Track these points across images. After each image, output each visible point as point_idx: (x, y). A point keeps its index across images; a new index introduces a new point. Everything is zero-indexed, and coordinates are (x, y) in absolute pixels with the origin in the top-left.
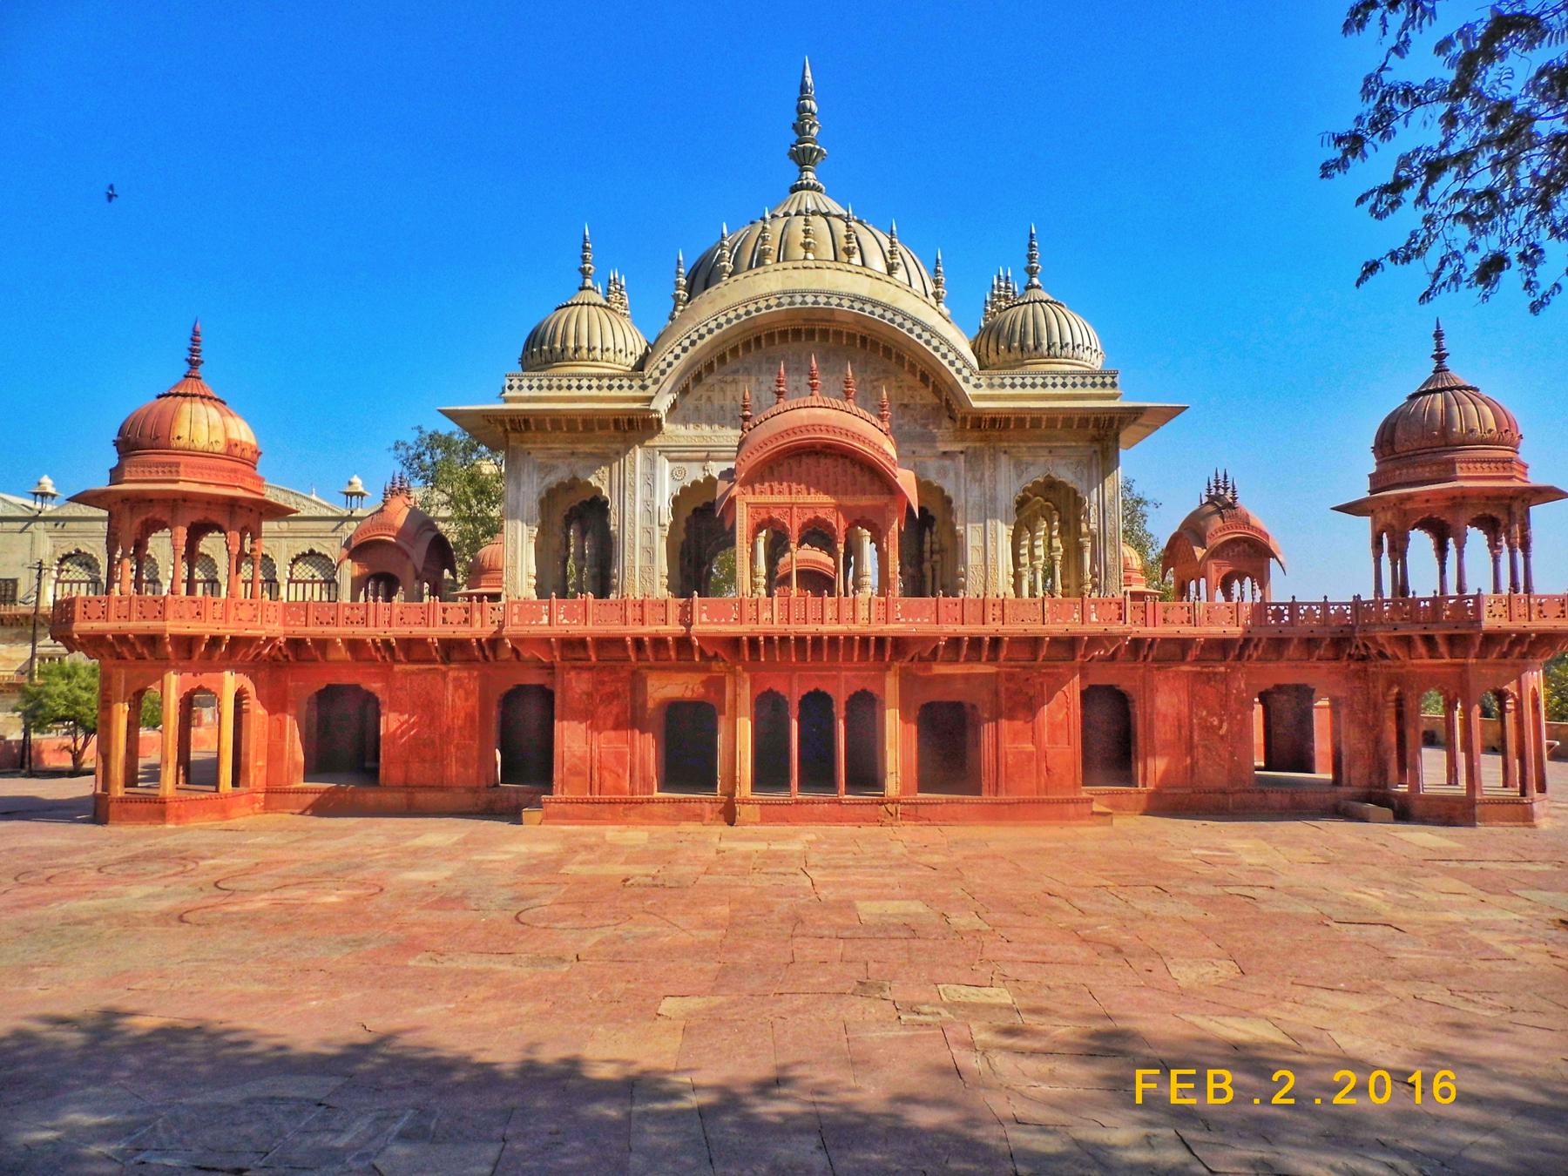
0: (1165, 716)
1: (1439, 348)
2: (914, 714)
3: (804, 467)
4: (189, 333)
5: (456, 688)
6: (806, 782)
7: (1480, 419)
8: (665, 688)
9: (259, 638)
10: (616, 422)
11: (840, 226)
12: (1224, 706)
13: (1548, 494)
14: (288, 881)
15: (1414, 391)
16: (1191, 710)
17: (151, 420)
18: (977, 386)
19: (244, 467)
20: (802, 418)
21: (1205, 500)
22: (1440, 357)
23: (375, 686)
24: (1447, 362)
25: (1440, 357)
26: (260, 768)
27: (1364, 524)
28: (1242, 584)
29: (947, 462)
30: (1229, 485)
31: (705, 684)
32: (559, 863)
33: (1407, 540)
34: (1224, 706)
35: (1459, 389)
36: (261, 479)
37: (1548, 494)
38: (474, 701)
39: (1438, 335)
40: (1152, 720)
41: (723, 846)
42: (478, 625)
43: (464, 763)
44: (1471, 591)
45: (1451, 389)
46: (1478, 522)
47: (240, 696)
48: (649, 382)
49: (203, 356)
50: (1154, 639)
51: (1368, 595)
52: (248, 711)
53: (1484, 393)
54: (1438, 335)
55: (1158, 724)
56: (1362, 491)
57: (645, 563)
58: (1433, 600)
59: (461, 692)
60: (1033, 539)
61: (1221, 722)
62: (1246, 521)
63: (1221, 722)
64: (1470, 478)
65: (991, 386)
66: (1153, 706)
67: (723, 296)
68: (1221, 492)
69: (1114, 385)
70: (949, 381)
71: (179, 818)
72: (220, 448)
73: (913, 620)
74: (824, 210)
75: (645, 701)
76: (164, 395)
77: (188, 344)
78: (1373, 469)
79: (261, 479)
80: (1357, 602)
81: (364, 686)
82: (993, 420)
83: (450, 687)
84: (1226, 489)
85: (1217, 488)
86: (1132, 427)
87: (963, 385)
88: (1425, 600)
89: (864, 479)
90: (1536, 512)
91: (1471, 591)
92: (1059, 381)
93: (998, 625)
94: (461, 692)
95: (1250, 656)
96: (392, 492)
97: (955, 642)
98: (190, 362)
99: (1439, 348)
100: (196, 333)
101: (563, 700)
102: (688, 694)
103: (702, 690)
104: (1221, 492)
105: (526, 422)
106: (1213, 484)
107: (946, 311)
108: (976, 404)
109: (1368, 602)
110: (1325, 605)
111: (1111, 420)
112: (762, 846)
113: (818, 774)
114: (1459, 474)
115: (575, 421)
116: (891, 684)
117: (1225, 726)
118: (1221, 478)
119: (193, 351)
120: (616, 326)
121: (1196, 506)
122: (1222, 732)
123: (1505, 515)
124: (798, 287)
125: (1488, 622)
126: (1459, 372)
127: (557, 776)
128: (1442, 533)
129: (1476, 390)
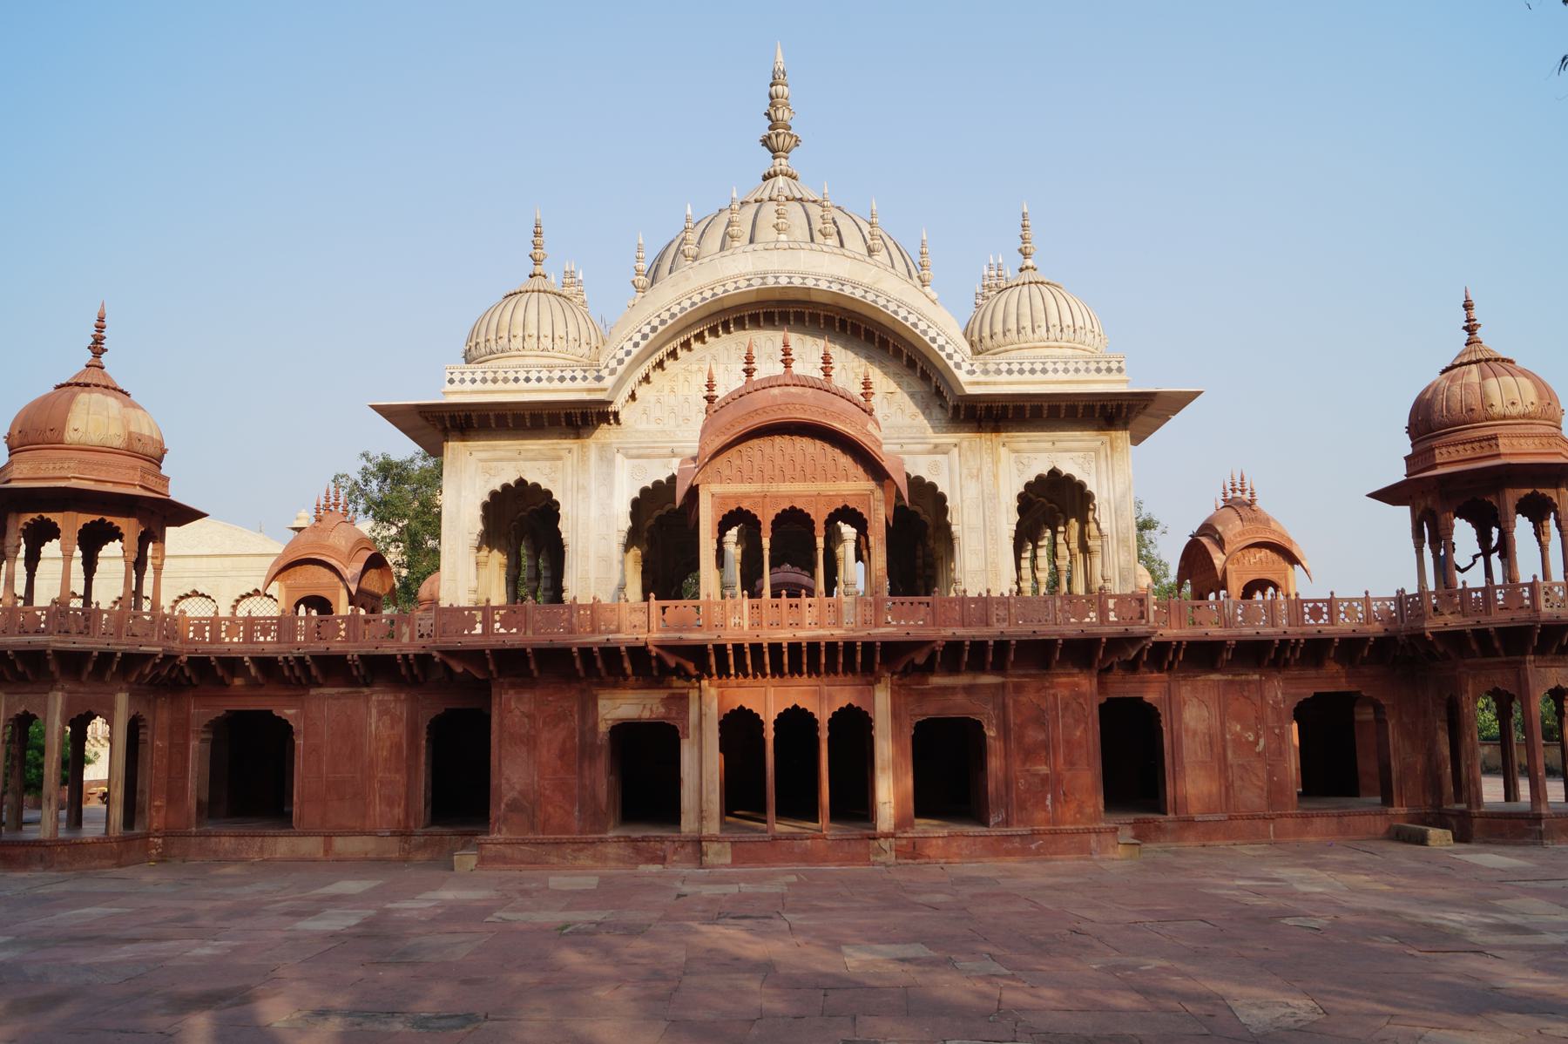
0: (1195, 733)
2: (909, 732)
3: (777, 447)
4: (94, 321)
5: (381, 714)
6: (742, 645)
8: (622, 706)
9: (154, 655)
10: (568, 416)
11: (815, 211)
12: (1260, 719)
16: (1223, 724)
18: (972, 372)
19: (147, 464)
20: (775, 397)
21: (1222, 504)
22: (1471, 328)
23: (288, 713)
24: (1480, 333)
25: (1471, 328)
27: (1404, 512)
29: (939, 457)
30: (1247, 486)
31: (666, 702)
32: (488, 910)
33: (1453, 526)
34: (1260, 719)
35: (1496, 360)
36: (167, 479)
38: (401, 729)
39: (1468, 306)
40: (1179, 737)
41: (686, 889)
42: (406, 639)
43: (390, 802)
45: (1487, 360)
46: (1526, 508)
48: (605, 373)
49: (106, 344)
50: (1179, 643)
51: (1412, 589)
54: (1468, 306)
55: (1187, 742)
56: (1398, 474)
57: (598, 562)
58: (1484, 590)
59: (387, 719)
60: (1035, 547)
61: (1258, 737)
62: (1267, 521)
63: (1258, 737)
65: (986, 372)
66: (1180, 719)
67: (688, 279)
68: (1238, 494)
69: (1120, 370)
70: (940, 366)
72: (117, 443)
73: (900, 623)
74: (798, 196)
75: (596, 724)
76: (62, 386)
77: (93, 331)
78: (1409, 451)
79: (167, 479)
80: (1401, 598)
81: (276, 713)
82: (989, 409)
83: (374, 712)
84: (1243, 491)
85: (1233, 491)
86: (1141, 418)
87: (956, 371)
88: (1476, 590)
89: (845, 461)
92: (1060, 366)
93: (1003, 627)
94: (387, 719)
95: (1287, 661)
96: (327, 508)
97: (954, 646)
100: (101, 319)
101: (501, 724)
102: (646, 715)
103: (662, 710)
104: (1238, 494)
105: (468, 418)
106: (1229, 487)
107: (934, 296)
108: (970, 390)
109: (1413, 596)
110: (1367, 600)
111: (1119, 407)
112: (732, 889)
113: (798, 805)
115: (523, 416)
116: (881, 703)
117: (1262, 742)
118: (1238, 480)
120: (568, 313)
121: (1211, 511)
122: (1260, 748)
124: (770, 268)
126: (1492, 340)
127: (493, 814)
128: (1486, 519)
129: (1511, 361)
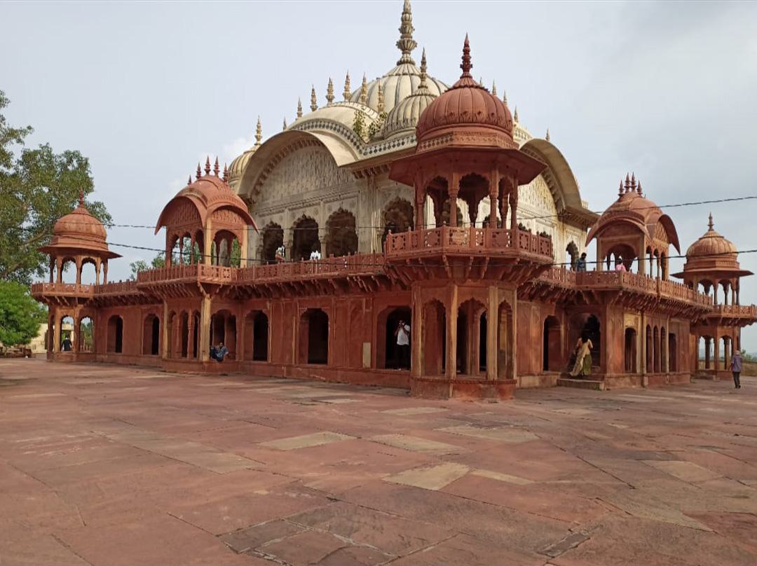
1: (711, 222)
7: (722, 247)
13: (748, 273)
14: (602, 401)
15: (701, 237)
17: (443, 108)
22: (711, 225)
24: (713, 227)
25: (711, 225)
28: (715, 289)
37: (748, 273)
39: (710, 218)
44: (719, 303)
46: (702, 282)
47: (503, 307)
53: (725, 238)
54: (710, 218)
64: (721, 266)
71: (553, 370)
90: (742, 280)
91: (719, 303)
98: (256, 137)
99: (711, 222)
114: (717, 265)
119: (258, 132)
123: (731, 278)
125: (724, 315)
129: (723, 237)
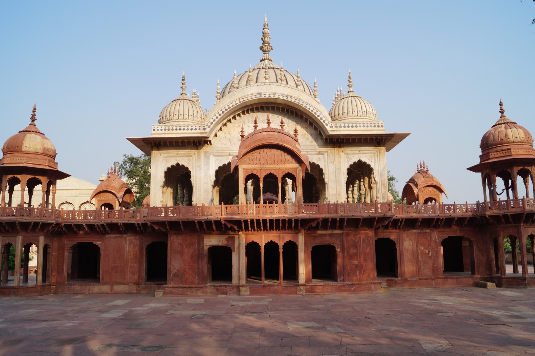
0: (408, 250)
2: (310, 250)
3: (265, 153)
4: (32, 109)
5: (130, 243)
8: (212, 241)
9: (52, 223)
10: (194, 142)
11: (278, 72)
12: (430, 245)
16: (417, 247)
18: (332, 127)
19: (50, 158)
20: (264, 135)
21: (417, 172)
22: (502, 112)
23: (98, 243)
24: (505, 114)
25: (502, 112)
26: (54, 276)
27: (479, 175)
29: (320, 156)
30: (426, 166)
31: (227, 239)
33: (496, 179)
34: (430, 245)
35: (511, 123)
36: (57, 163)
38: (137, 248)
39: (501, 104)
40: (402, 251)
41: (234, 303)
42: (138, 218)
43: (133, 274)
45: (507, 123)
46: (521, 173)
48: (206, 127)
49: (36, 117)
50: (402, 219)
51: (482, 201)
52: (50, 253)
54: (501, 104)
55: (405, 253)
56: (477, 162)
57: (204, 192)
58: (506, 201)
59: (132, 245)
60: (353, 187)
61: (429, 251)
62: (432, 178)
63: (429, 251)
65: (336, 127)
66: (403, 245)
67: (235, 95)
68: (422, 168)
69: (382, 126)
70: (321, 125)
72: (40, 151)
73: (307, 212)
74: (272, 67)
75: (203, 247)
76: (21, 132)
77: (32, 113)
78: (481, 154)
79: (57, 163)
80: (478, 204)
81: (94, 243)
82: (337, 139)
83: (128, 243)
84: (424, 167)
85: (421, 167)
86: (389, 142)
87: (326, 127)
88: (504, 201)
89: (288, 157)
92: (362, 125)
93: (342, 214)
94: (132, 245)
95: (439, 225)
96: (112, 173)
97: (325, 220)
100: (34, 109)
101: (171, 247)
102: (220, 244)
103: (226, 242)
104: (422, 168)
105: (160, 142)
106: (419, 166)
107: (319, 101)
108: (331, 133)
109: (482, 203)
110: (466, 205)
111: (382, 139)
112: (250, 303)
113: (272, 274)
115: (178, 142)
116: (301, 240)
117: (431, 253)
118: (422, 164)
120: (194, 107)
121: (413, 174)
122: (430, 255)
124: (263, 91)
126: (509, 116)
127: (168, 277)
128: (507, 177)
129: (516, 123)
